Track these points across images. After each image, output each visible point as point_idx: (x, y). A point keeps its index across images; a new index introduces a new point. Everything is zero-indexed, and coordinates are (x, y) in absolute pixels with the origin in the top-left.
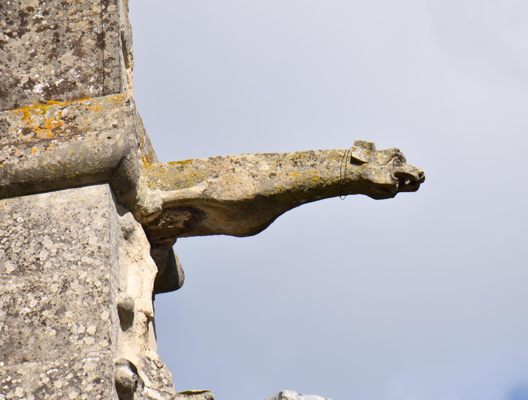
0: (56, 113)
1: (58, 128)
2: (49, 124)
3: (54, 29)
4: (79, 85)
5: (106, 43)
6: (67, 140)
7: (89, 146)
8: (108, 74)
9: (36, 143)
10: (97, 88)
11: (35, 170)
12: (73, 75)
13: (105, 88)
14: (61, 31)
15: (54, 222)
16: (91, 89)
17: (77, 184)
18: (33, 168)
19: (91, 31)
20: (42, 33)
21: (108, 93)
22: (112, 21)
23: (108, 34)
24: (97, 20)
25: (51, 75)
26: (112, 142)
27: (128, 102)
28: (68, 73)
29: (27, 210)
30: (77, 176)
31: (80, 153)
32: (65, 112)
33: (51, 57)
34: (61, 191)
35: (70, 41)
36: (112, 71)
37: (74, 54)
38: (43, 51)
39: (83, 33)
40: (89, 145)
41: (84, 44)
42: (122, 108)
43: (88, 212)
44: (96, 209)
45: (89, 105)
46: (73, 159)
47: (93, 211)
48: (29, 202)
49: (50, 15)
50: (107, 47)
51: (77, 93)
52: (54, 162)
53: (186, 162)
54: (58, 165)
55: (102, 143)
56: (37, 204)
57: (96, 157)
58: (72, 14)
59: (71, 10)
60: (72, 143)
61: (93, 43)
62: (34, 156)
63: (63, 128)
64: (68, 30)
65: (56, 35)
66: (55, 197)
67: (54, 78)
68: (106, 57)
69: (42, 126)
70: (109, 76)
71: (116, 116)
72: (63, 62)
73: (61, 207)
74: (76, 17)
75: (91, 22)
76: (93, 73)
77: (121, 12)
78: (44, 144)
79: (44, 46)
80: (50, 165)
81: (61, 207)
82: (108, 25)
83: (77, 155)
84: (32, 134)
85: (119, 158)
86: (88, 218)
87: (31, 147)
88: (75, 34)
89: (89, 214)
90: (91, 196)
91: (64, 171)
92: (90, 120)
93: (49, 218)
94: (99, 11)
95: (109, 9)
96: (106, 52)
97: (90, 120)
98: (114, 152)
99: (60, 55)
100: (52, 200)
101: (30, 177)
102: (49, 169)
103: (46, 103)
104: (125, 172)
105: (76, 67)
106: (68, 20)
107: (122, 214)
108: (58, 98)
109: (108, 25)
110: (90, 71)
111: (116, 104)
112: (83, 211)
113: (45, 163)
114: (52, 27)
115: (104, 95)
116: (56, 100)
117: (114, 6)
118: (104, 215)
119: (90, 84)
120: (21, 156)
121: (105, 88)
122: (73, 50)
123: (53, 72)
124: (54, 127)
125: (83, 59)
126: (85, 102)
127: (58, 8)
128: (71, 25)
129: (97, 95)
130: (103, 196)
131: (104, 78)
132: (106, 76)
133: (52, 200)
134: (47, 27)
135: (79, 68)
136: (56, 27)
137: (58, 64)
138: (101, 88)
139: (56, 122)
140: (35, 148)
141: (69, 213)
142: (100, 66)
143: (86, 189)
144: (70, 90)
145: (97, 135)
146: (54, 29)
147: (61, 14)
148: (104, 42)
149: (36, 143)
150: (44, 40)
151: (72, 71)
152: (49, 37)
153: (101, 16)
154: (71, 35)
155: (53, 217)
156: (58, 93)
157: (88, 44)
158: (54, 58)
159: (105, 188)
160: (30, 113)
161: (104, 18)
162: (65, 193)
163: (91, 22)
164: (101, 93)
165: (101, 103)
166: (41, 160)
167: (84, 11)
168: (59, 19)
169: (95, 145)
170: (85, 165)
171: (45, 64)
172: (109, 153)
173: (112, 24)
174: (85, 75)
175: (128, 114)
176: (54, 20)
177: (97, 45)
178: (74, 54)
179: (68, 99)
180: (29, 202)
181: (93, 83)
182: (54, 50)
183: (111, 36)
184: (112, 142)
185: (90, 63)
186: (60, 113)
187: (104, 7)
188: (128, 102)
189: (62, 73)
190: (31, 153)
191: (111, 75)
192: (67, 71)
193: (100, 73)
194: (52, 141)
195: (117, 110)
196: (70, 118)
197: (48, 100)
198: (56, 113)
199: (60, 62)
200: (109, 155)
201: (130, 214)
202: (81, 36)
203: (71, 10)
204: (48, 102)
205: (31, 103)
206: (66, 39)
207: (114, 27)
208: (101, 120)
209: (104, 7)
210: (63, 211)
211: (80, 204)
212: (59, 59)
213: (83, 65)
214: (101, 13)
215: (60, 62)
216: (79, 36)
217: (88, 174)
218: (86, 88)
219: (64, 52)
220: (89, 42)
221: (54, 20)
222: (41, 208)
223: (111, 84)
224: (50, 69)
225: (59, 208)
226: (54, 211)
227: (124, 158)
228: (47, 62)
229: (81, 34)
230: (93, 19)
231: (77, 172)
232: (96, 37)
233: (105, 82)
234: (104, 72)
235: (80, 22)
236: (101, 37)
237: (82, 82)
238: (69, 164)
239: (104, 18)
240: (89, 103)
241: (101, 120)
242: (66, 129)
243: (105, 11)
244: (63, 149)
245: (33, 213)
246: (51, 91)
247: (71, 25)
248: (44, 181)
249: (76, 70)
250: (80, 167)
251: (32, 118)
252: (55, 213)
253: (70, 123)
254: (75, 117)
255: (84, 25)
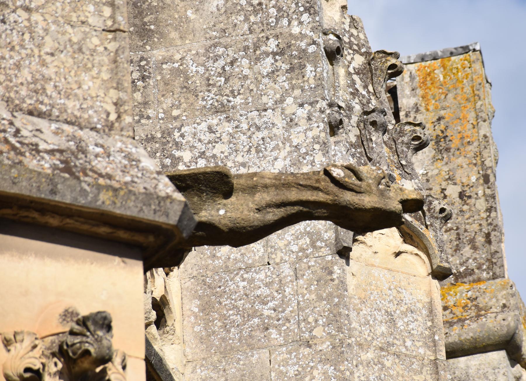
0: (464, 295)
1: (466, 306)
2: (460, 303)
3: (456, 230)
4: (476, 271)
5: (492, 240)
6: (476, 321)
7: (491, 326)
8: (495, 263)
9: (455, 323)
10: (488, 273)
11: (456, 343)
12: (471, 264)
13: (494, 274)
14: (461, 231)
15: (471, 379)
16: (485, 274)
17: (484, 351)
18: (455, 342)
19: (481, 231)
20: (448, 233)
21: (497, 278)
22: (494, 224)
23: (493, 233)
24: (484, 223)
25: (457, 264)
26: (506, 323)
27: (511, 286)
28: (468, 262)
29: (453, 369)
30: (484, 346)
31: (486, 331)
32: (470, 293)
33: (456, 251)
34: (474, 356)
35: (468, 239)
36: (498, 261)
37: (471, 248)
38: (450, 246)
39: (476, 232)
40: (491, 325)
41: (477, 241)
42: (508, 291)
43: (493, 371)
44: (498, 370)
45: (486, 289)
46: (481, 335)
47: (496, 371)
48: (453, 364)
49: (453, 220)
50: (493, 243)
51: (475, 277)
52: (468, 337)
53: (390, 54)
54: (471, 339)
55: (500, 323)
56: (459, 365)
57: (496, 333)
58: (467, 219)
59: (467, 215)
60: (479, 323)
61: (483, 240)
62: (455, 333)
63: (469, 305)
64: (466, 231)
65: (458, 234)
66: (470, 360)
67: (459, 266)
68: (493, 251)
69: (456, 305)
70: (496, 265)
71: (504, 297)
72: (464, 254)
73: (475, 367)
74: (470, 221)
75: (480, 225)
76: (484, 262)
77: (499, 215)
78: (461, 324)
79: (450, 242)
80: (466, 340)
81: (475, 367)
82: (492, 227)
83: (484, 333)
84: (450, 310)
85: (512, 334)
86: (494, 376)
87: (452, 326)
88: (470, 234)
89: (494, 373)
90: (494, 359)
91: (476, 343)
92: (487, 300)
93: (468, 376)
94: (485, 217)
95: (492, 215)
96: (492, 247)
97: (487, 300)
98: (508, 330)
99: (462, 249)
100: (468, 362)
101: (453, 348)
102: (466, 342)
103: (455, 285)
104: (515, 341)
105: (473, 258)
106: (465, 223)
107: (513, 366)
108: (463, 281)
109: (492, 227)
110: (482, 261)
111: (503, 287)
112: (490, 370)
113: (462, 338)
114: (455, 228)
115: (494, 279)
116: (462, 283)
117: (495, 213)
118: (504, 374)
119: (484, 270)
120: (447, 333)
121: (494, 274)
122: (470, 246)
123: (458, 262)
124: (463, 305)
125: (478, 252)
126: (482, 286)
127: (457, 215)
128: (468, 227)
129: (489, 279)
130: (502, 359)
131: (493, 266)
132: (494, 265)
133: (468, 362)
134: (451, 229)
135: (475, 259)
136: (458, 228)
137: (461, 256)
138: (491, 274)
139: (465, 301)
140: (455, 327)
141: (480, 372)
142: (489, 257)
143: (490, 354)
144: (471, 275)
145: (495, 317)
146: (456, 230)
147: (460, 218)
148: (490, 239)
149: (455, 323)
150: (450, 238)
151: (471, 261)
152: (453, 236)
153: (487, 220)
154: (468, 234)
155: (470, 375)
156: (463, 277)
157: (480, 241)
158: (458, 251)
159: (502, 354)
160: (447, 295)
161: (489, 221)
162: (476, 357)
163: (480, 225)
164: (491, 277)
165: (493, 287)
166: (460, 336)
167: (475, 217)
168: (459, 222)
169: (494, 324)
170: (489, 339)
171: (452, 256)
172: (505, 330)
173: (495, 226)
174: (480, 264)
175: (513, 295)
176: (456, 223)
177: (486, 241)
178: (471, 248)
179: (470, 281)
180: (453, 364)
181: (485, 270)
182: (457, 245)
183: (495, 235)
184: (506, 323)
185: (482, 255)
186: (467, 295)
187: (488, 214)
188: (511, 286)
189: (464, 262)
190: (453, 331)
191: (497, 264)
192: (467, 261)
193: (490, 262)
194: (466, 322)
195: (505, 292)
196: (474, 299)
197: (457, 282)
198: (464, 295)
199: (462, 254)
200: (505, 332)
201: (518, 365)
202: (475, 235)
203: (467, 215)
204: (457, 284)
205: (445, 285)
206: (465, 237)
207: (496, 228)
208: (494, 300)
209: (488, 214)
210: (477, 370)
211: (487, 365)
212: (461, 252)
213: (478, 256)
214: (486, 218)
215: (462, 254)
216: (473, 235)
217: (491, 345)
218: (481, 273)
219: (464, 247)
220: (480, 239)
221: (456, 223)
222: (462, 368)
223: (498, 271)
224: (456, 260)
225: (474, 368)
226: (470, 371)
227: (515, 333)
228: (454, 255)
229: (474, 233)
230: (482, 223)
231: (484, 344)
232: (484, 236)
233: (494, 269)
234: (492, 262)
235: (473, 225)
236: (488, 235)
237: (478, 269)
238: (479, 338)
239: (489, 221)
240: (485, 287)
241: (494, 300)
242: (471, 306)
243: (489, 216)
244: (474, 329)
245: (457, 372)
246: (458, 276)
247: (468, 227)
248: (463, 350)
249: (474, 260)
250: (486, 340)
251: (448, 298)
252: (472, 372)
253: (474, 302)
254: (477, 298)
255: (476, 227)
